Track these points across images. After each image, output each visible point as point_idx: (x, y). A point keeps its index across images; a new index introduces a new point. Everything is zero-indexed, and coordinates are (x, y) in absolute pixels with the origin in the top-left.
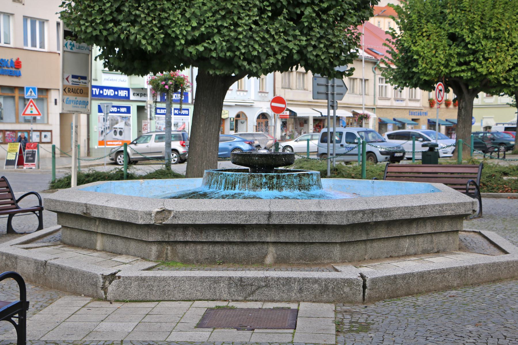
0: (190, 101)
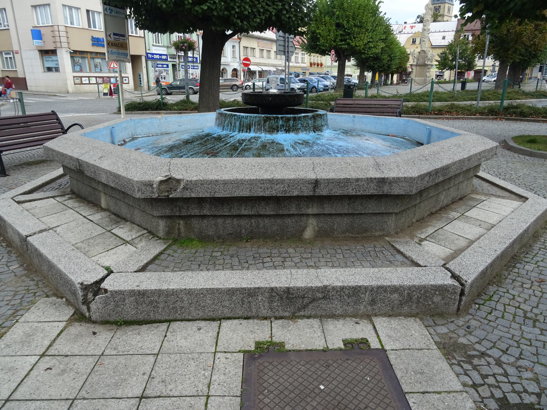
0: (199, 62)
